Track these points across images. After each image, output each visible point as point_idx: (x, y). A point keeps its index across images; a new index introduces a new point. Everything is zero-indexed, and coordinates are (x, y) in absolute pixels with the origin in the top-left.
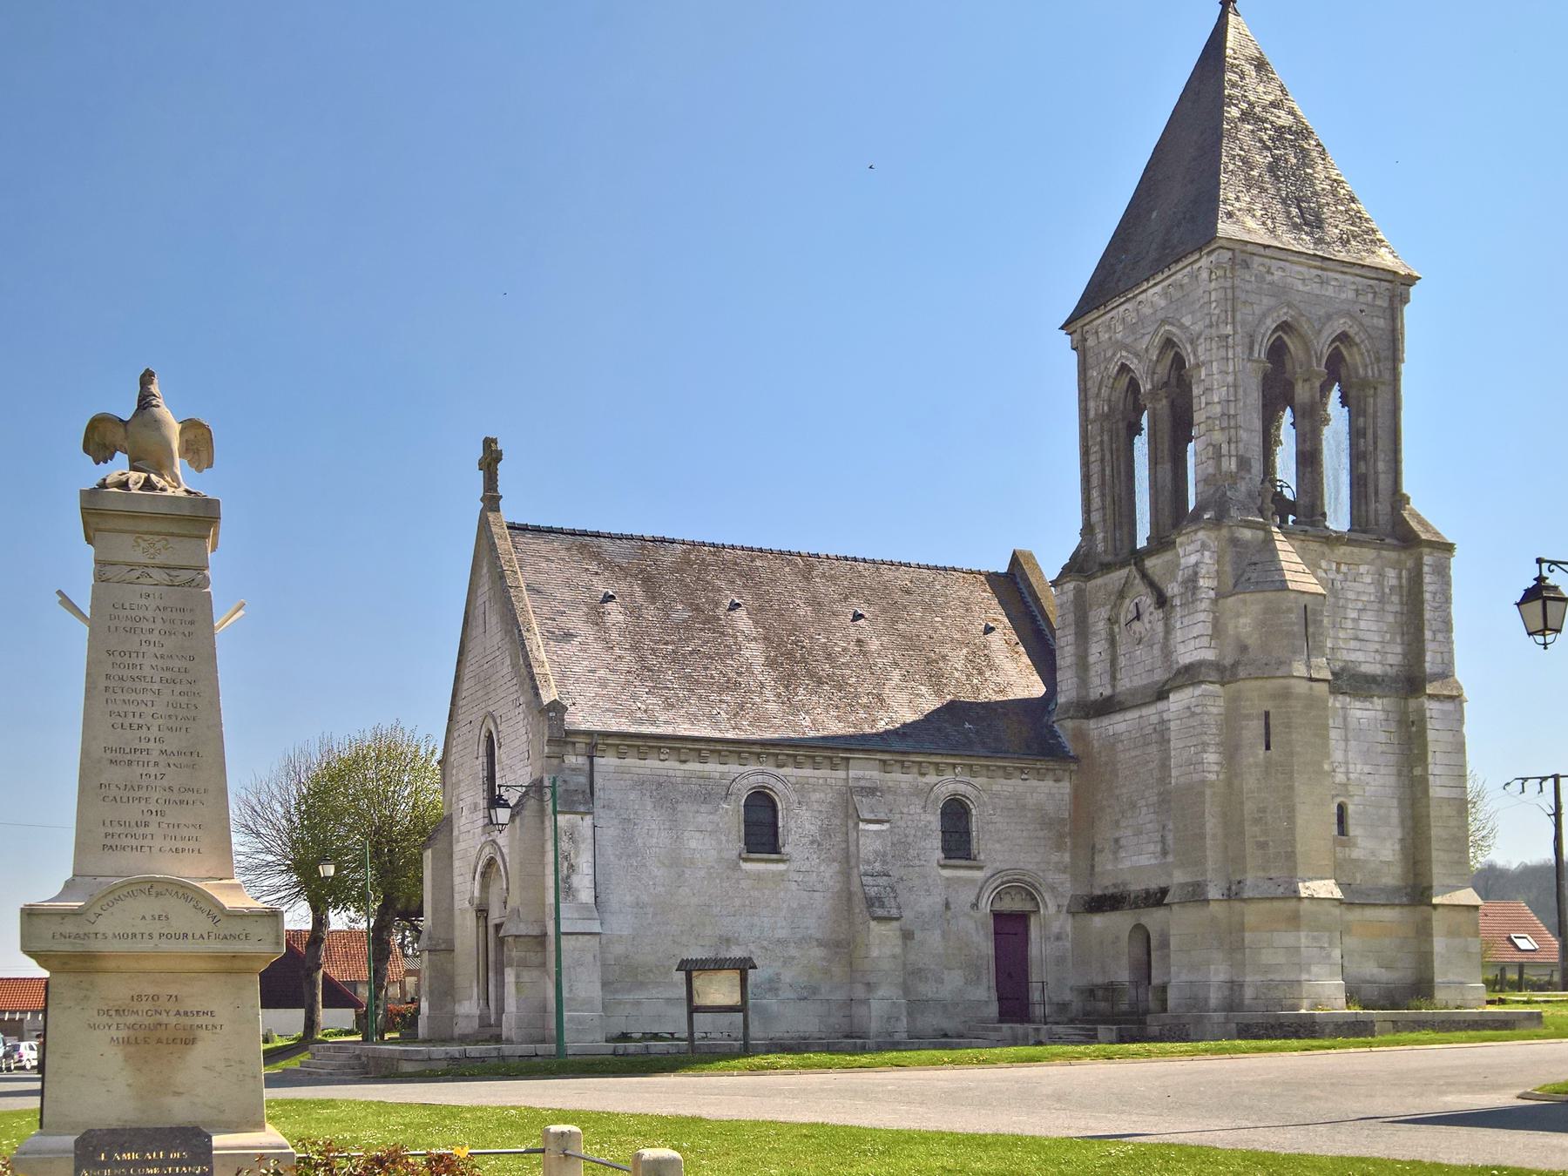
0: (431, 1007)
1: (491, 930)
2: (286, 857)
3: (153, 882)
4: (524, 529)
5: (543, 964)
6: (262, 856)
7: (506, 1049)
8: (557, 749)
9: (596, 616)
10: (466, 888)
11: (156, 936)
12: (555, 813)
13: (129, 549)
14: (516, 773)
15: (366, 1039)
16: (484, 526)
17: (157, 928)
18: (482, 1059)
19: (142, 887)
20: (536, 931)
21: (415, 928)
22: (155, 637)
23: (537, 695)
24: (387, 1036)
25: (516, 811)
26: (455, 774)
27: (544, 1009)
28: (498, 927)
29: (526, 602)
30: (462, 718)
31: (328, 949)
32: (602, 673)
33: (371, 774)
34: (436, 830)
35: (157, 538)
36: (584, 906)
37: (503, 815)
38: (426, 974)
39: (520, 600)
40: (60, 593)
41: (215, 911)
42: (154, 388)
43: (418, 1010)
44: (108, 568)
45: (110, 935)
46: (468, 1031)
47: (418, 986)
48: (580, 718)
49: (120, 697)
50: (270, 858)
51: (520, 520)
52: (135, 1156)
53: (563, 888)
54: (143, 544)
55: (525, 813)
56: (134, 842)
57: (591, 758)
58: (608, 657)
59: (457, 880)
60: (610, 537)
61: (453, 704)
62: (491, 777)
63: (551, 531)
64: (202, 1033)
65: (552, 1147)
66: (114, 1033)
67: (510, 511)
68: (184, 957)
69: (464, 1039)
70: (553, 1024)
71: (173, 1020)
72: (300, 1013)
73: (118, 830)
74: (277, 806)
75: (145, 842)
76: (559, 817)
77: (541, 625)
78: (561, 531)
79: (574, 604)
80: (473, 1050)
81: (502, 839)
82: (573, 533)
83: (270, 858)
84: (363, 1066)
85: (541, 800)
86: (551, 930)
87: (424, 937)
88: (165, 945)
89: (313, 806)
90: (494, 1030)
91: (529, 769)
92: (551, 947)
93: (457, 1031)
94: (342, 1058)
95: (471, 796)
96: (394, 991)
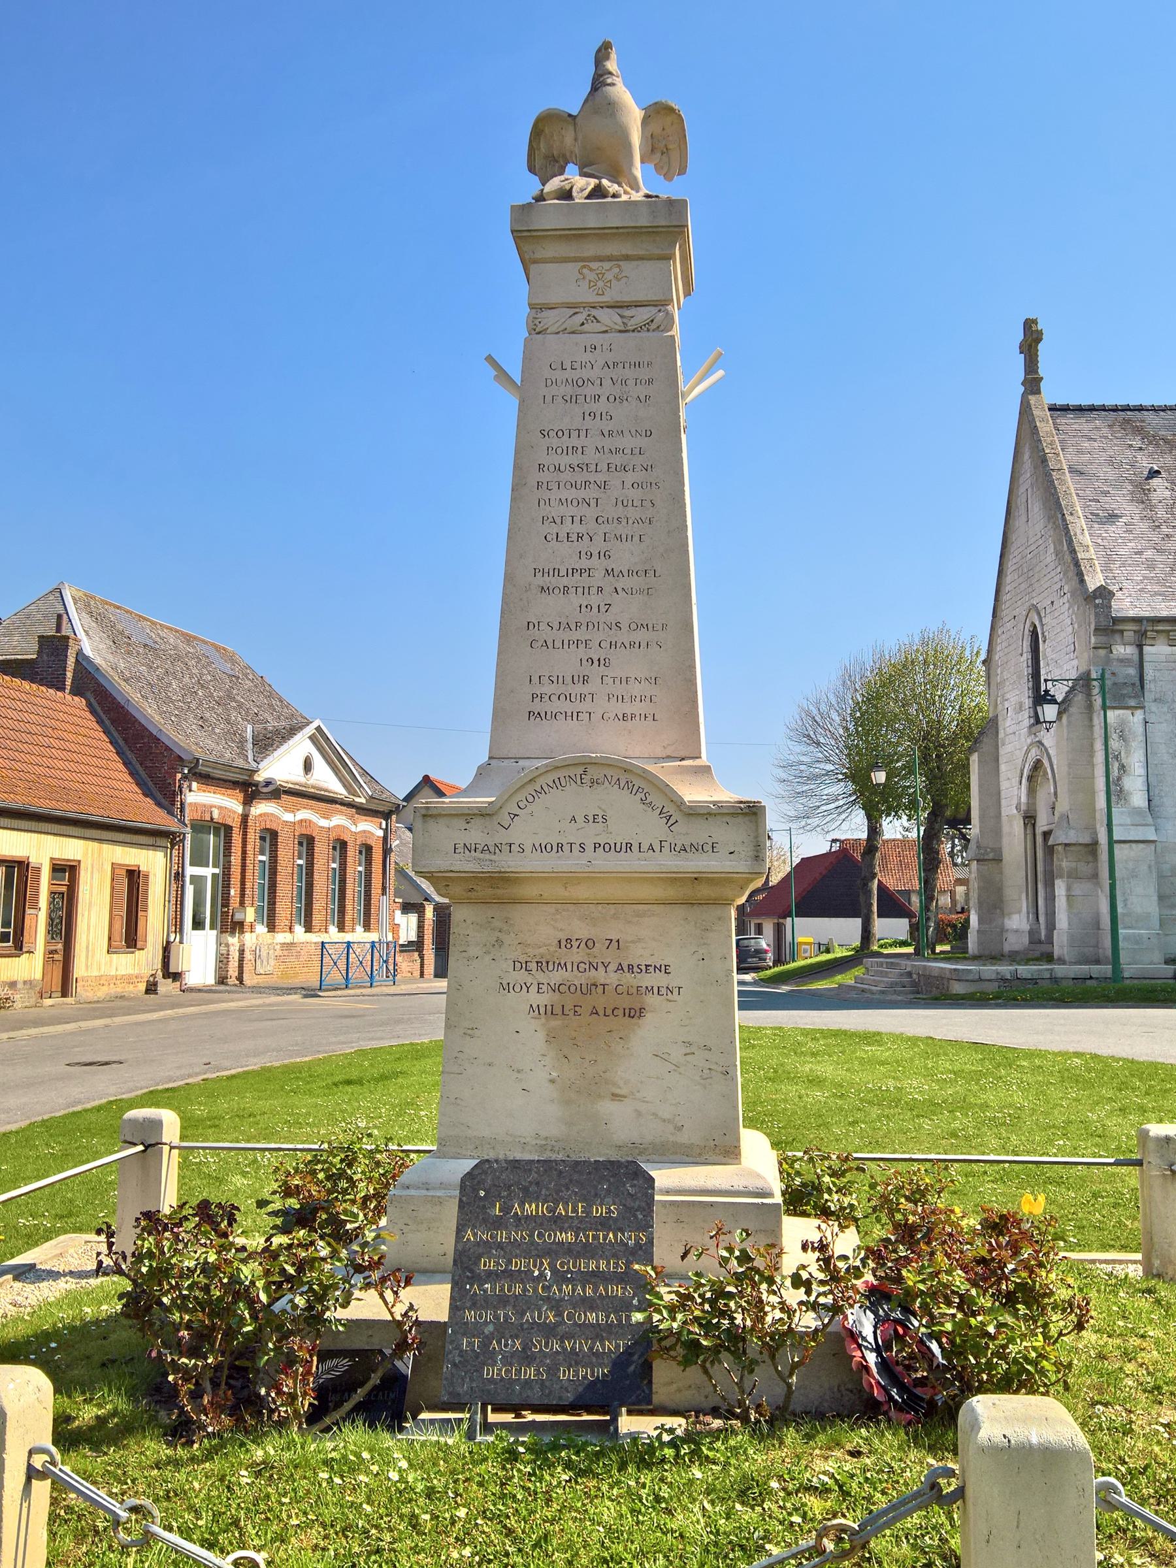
0: (980, 921)
1: (1039, 839)
2: (843, 766)
3: (586, 764)
4: (1065, 409)
5: (1095, 876)
6: (822, 766)
7: (1060, 970)
8: (1103, 639)
9: (1141, 494)
10: (1013, 792)
11: (589, 848)
12: (1105, 708)
13: (566, 283)
14: (1063, 665)
15: (918, 952)
16: (1025, 410)
17: (591, 834)
18: (1034, 981)
19: (571, 772)
20: (1086, 839)
21: (963, 837)
22: (602, 406)
23: (1082, 581)
24: (938, 949)
25: (1064, 707)
26: (1000, 674)
27: (1097, 925)
28: (1046, 835)
29: (1068, 485)
30: (1006, 613)
31: (884, 858)
32: (1149, 554)
33: (919, 678)
34: (982, 733)
35: (607, 265)
36: (1137, 811)
37: (1050, 712)
38: (974, 885)
39: (1063, 482)
40: (490, 359)
41: (670, 809)
42: (612, 65)
43: (967, 921)
44: (546, 313)
45: (528, 848)
46: (1016, 948)
47: (967, 895)
48: (1125, 605)
49: (555, 495)
50: (830, 767)
51: (1060, 402)
52: (543, 1209)
53: (1115, 791)
54: (591, 276)
55: (1072, 710)
56: (568, 707)
57: (1140, 647)
58: (1156, 538)
59: (1004, 785)
60: (1154, 409)
61: (997, 599)
62: (1036, 675)
63: (1092, 408)
64: (651, 1000)
65: (1153, 1158)
66: (535, 998)
67: (1052, 392)
68: (630, 880)
69: (1014, 957)
70: (1107, 942)
71: (613, 978)
72: (858, 922)
73: (548, 689)
74: (835, 716)
75: (584, 707)
76: (1110, 713)
77: (1084, 507)
78: (1103, 408)
79: (1118, 484)
80: (1024, 970)
81: (1049, 739)
82: (1115, 409)
83: (830, 767)
84: (915, 984)
85: (1089, 695)
86: (1103, 839)
87: (972, 845)
88: (605, 862)
89: (866, 711)
90: (1044, 948)
91: (1075, 662)
92: (1104, 856)
93: (1007, 948)
94: (893, 976)
95: (1017, 695)
96: (945, 900)
